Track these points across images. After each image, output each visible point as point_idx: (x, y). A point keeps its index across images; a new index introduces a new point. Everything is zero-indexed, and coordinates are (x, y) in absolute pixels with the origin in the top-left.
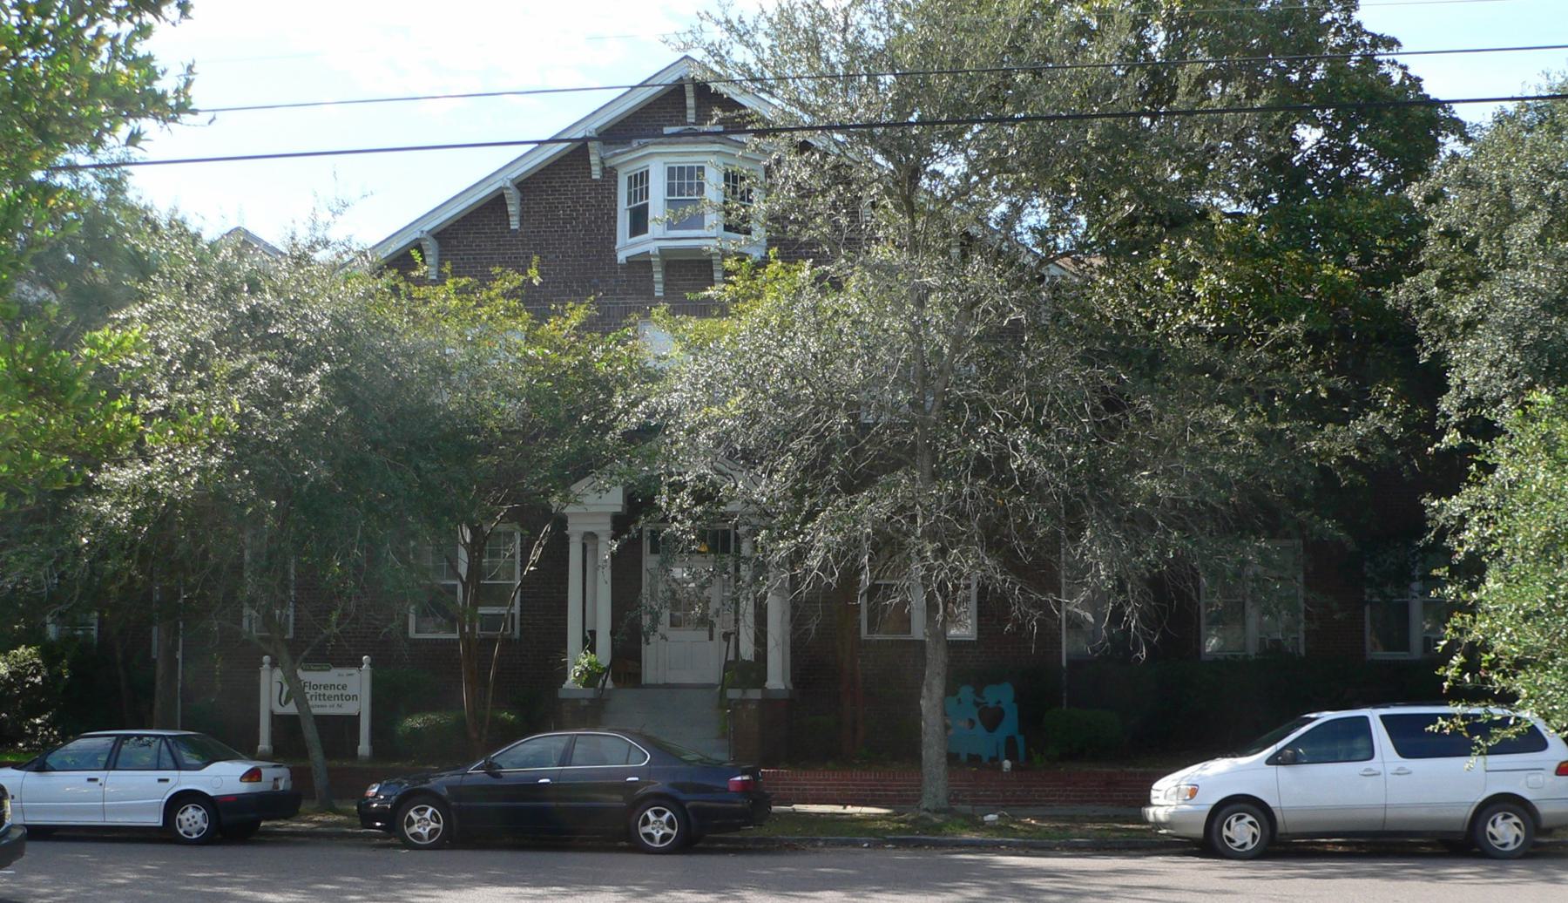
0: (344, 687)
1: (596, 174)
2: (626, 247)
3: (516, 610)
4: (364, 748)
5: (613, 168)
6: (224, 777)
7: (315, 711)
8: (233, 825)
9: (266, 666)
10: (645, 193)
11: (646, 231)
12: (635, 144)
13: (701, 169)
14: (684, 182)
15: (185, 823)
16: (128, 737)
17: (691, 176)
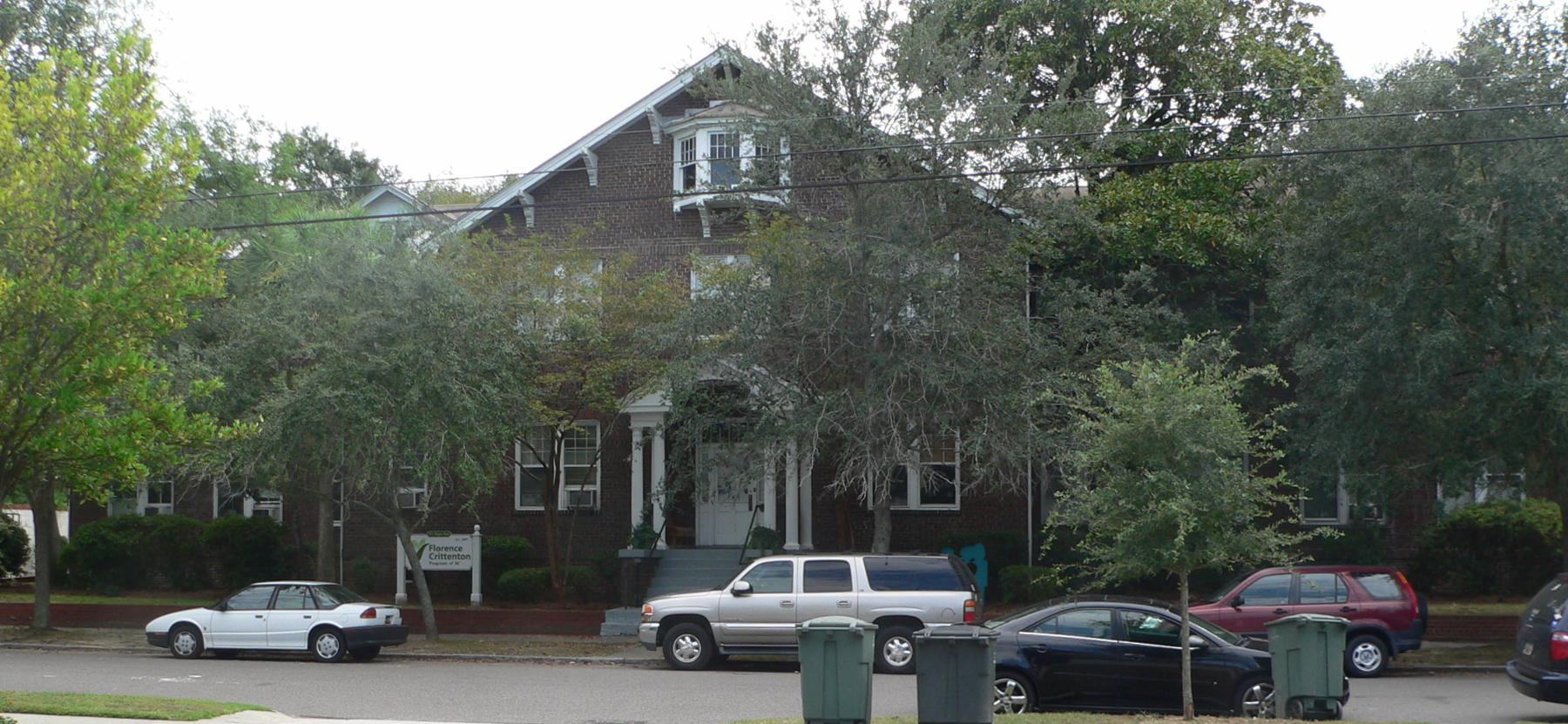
1: (657, 141)
3: (597, 487)
4: (476, 596)
6: (349, 615)
8: (359, 648)
10: (692, 155)
16: (288, 587)
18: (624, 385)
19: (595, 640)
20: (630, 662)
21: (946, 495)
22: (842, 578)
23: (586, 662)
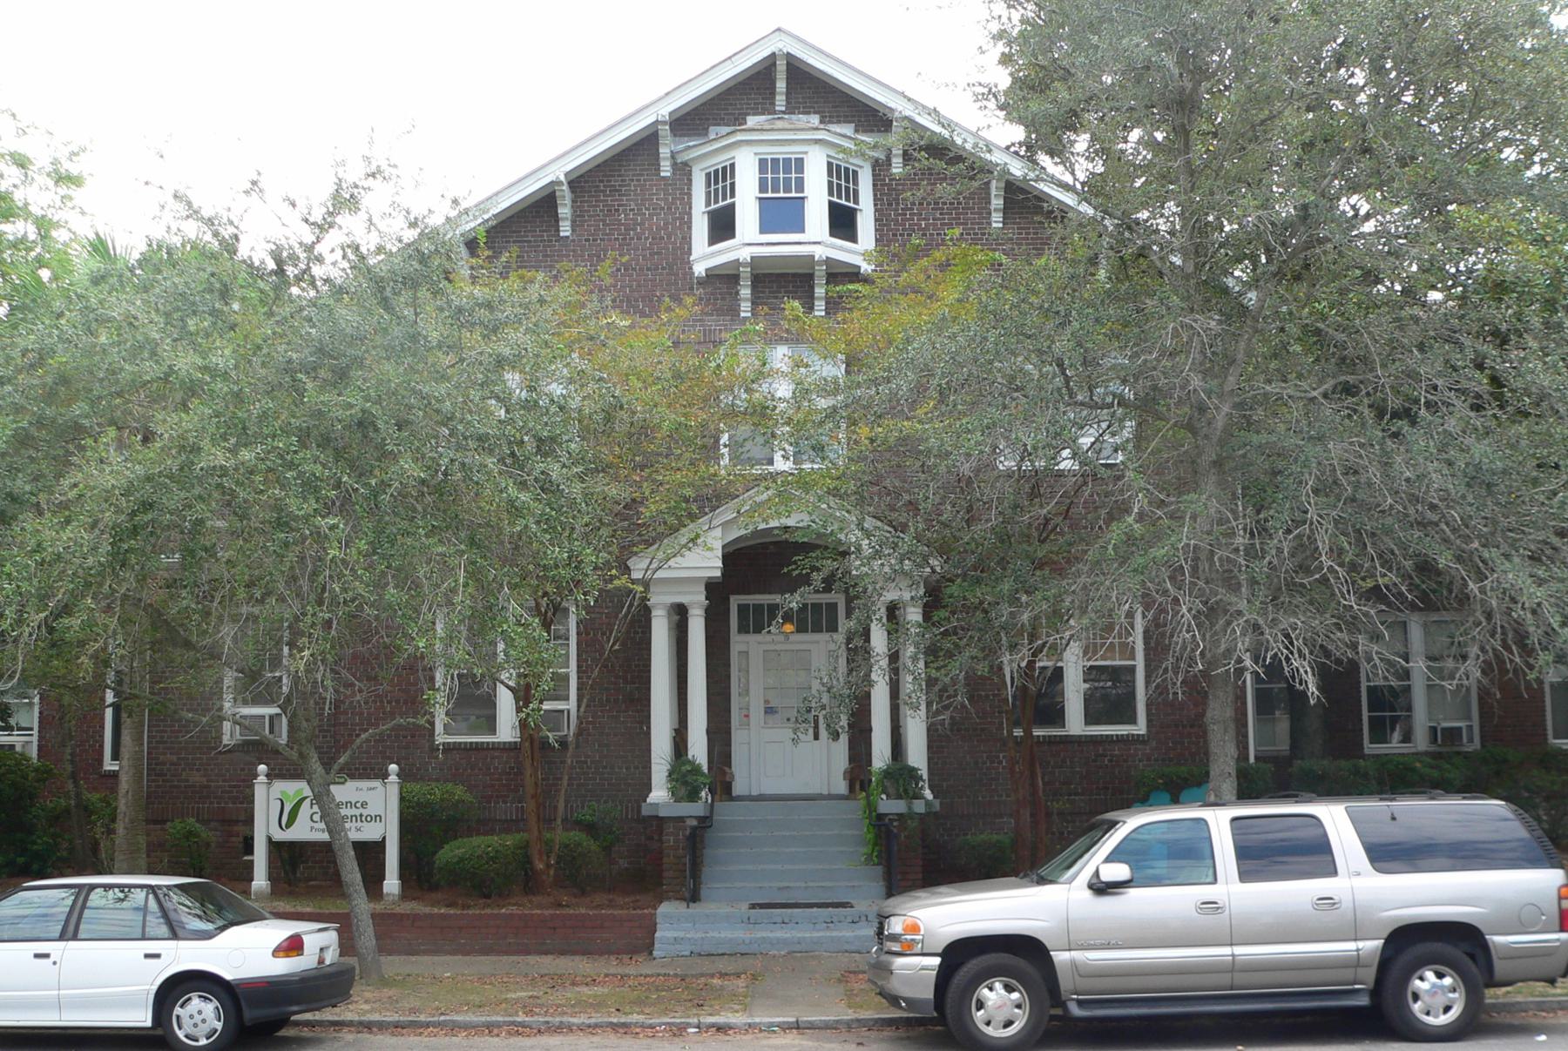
0: (365, 804)
1: (666, 170)
2: (705, 257)
3: (571, 705)
5: (685, 164)
7: (354, 836)
9: (262, 778)
11: (733, 236)
12: (713, 131)
13: (800, 163)
14: (781, 177)
15: (186, 1022)
16: (93, 887)
17: (787, 170)
18: (633, 530)
19: (637, 967)
20: (812, 1026)
21: (1121, 709)
22: (1314, 854)
23: (721, 1029)
